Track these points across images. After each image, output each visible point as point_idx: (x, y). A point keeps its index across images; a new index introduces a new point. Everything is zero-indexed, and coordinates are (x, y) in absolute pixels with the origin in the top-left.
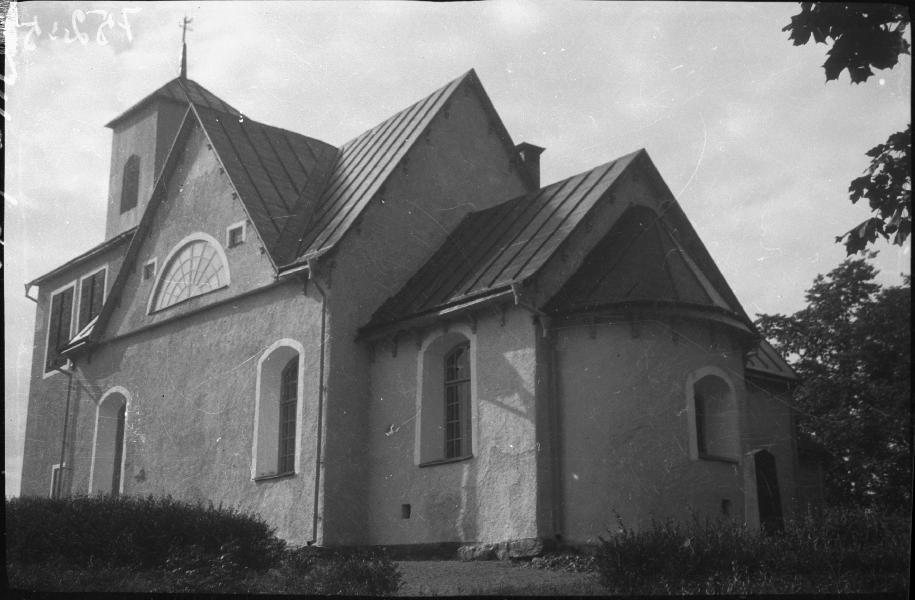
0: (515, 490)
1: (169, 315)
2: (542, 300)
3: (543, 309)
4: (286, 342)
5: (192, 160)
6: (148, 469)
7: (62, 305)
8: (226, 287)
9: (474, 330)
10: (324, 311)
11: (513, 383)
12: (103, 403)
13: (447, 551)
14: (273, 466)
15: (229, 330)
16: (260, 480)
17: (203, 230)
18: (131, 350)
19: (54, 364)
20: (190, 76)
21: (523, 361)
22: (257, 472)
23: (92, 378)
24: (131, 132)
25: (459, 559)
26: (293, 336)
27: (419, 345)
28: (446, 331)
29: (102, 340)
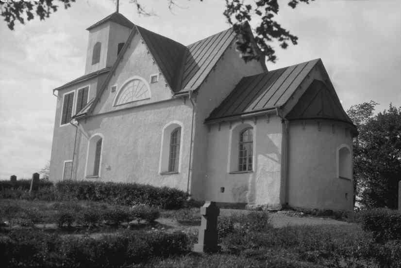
0: (271, 185)
1: (123, 107)
2: (285, 114)
3: (286, 117)
4: (175, 122)
5: (135, 48)
6: (111, 166)
7: (69, 99)
8: (149, 99)
9: (255, 123)
10: (193, 111)
11: (270, 148)
12: (93, 138)
13: (241, 206)
14: (167, 168)
15: (150, 116)
16: (162, 174)
17: (139, 75)
18: (105, 120)
19: (65, 121)
20: (120, 12)
21: (277, 139)
22: (161, 170)
23: (87, 130)
24: (97, 33)
25: (246, 209)
26: (179, 120)
27: (231, 127)
28: (243, 123)
29: (91, 115)
